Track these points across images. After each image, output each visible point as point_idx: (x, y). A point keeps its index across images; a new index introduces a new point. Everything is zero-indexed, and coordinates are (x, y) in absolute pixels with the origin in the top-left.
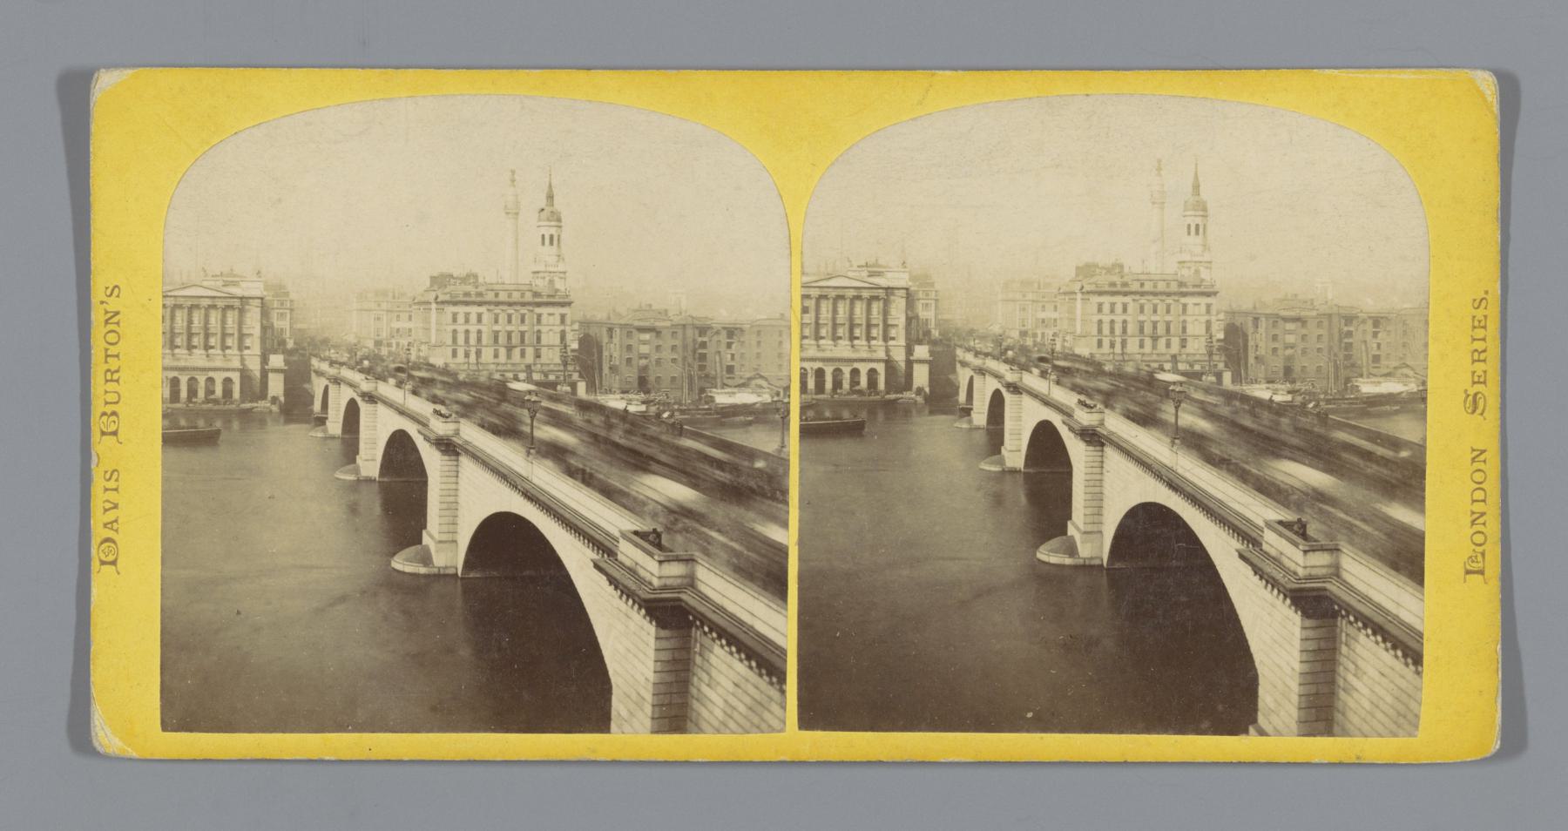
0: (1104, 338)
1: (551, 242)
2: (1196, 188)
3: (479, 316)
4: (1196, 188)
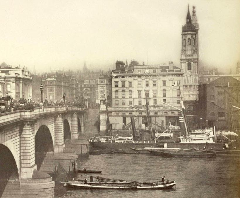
0: (157, 99)
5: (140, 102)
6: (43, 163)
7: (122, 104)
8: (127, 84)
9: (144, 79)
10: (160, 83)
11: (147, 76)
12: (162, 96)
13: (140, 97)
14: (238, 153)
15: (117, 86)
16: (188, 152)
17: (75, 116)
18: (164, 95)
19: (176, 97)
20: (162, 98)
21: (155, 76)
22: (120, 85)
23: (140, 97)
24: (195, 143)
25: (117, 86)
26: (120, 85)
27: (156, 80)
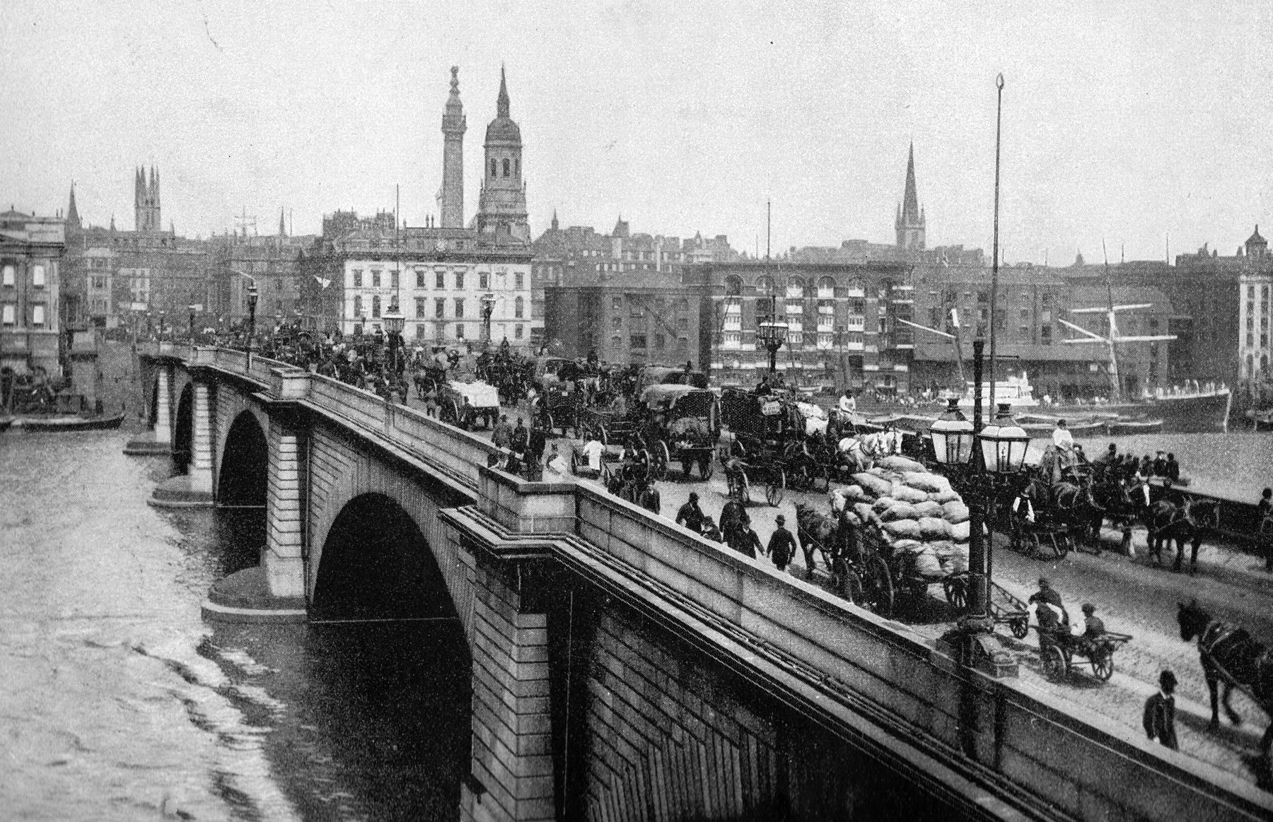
0: (465, 323)
1: (506, 174)
2: (503, 101)
3: (395, 274)
4: (503, 101)
5: (421, 330)
6: (552, 785)
7: (1006, 402)
8: (386, 278)
9: (414, 267)
10: (471, 280)
11: (441, 258)
12: (513, 317)
13: (420, 311)
14: (888, 709)
15: (358, 282)
16: (885, 711)
17: (239, 364)
18: (487, 313)
19: (514, 321)
20: (514, 321)
21: (461, 258)
22: (367, 279)
23: (420, 311)
24: (833, 596)
25: (358, 282)
26: (367, 279)
27: (443, 269)
